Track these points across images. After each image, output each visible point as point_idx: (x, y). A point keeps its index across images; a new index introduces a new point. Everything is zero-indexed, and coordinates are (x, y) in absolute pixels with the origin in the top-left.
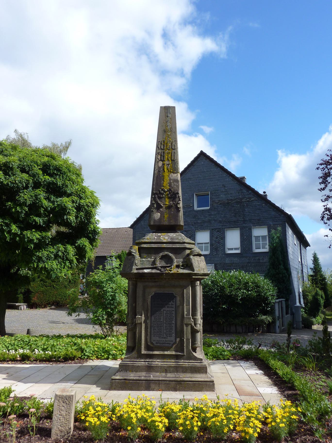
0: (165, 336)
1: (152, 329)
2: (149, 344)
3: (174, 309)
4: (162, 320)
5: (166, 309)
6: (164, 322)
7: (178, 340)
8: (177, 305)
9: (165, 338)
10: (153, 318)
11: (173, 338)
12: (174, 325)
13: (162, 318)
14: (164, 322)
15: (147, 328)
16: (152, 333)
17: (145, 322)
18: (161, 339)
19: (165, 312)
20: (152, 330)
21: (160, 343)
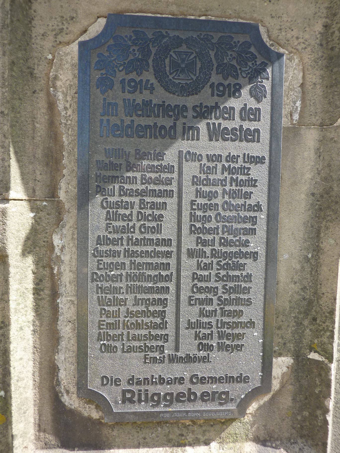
0: (189, 346)
1: (93, 297)
2: (71, 401)
3: (260, 149)
4: (168, 231)
5: (203, 145)
6: (189, 242)
7: (282, 365)
8: (285, 122)
9: (189, 359)
10: (96, 212)
11: (248, 361)
12: (255, 269)
13: (170, 215)
14: (189, 242)
15: (55, 294)
16: (93, 331)
17: (36, 243)
18: (158, 370)
19: (191, 169)
20: (93, 305)
21: (156, 399)
